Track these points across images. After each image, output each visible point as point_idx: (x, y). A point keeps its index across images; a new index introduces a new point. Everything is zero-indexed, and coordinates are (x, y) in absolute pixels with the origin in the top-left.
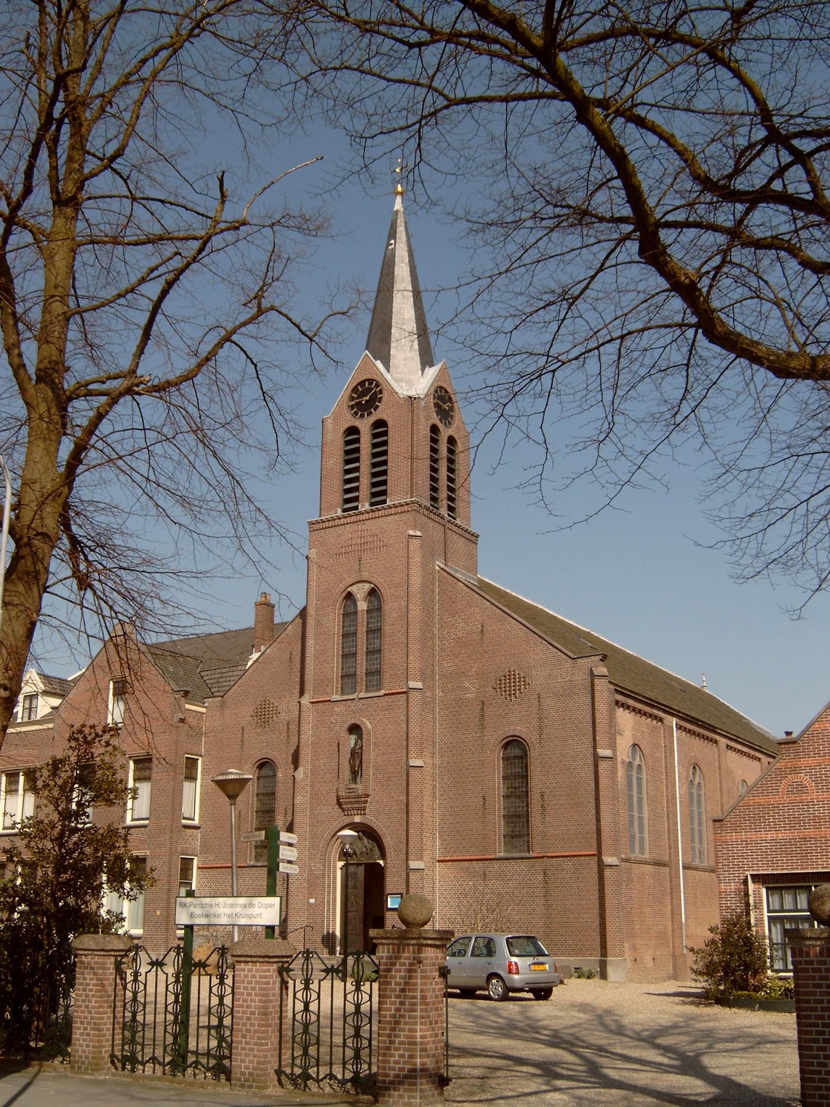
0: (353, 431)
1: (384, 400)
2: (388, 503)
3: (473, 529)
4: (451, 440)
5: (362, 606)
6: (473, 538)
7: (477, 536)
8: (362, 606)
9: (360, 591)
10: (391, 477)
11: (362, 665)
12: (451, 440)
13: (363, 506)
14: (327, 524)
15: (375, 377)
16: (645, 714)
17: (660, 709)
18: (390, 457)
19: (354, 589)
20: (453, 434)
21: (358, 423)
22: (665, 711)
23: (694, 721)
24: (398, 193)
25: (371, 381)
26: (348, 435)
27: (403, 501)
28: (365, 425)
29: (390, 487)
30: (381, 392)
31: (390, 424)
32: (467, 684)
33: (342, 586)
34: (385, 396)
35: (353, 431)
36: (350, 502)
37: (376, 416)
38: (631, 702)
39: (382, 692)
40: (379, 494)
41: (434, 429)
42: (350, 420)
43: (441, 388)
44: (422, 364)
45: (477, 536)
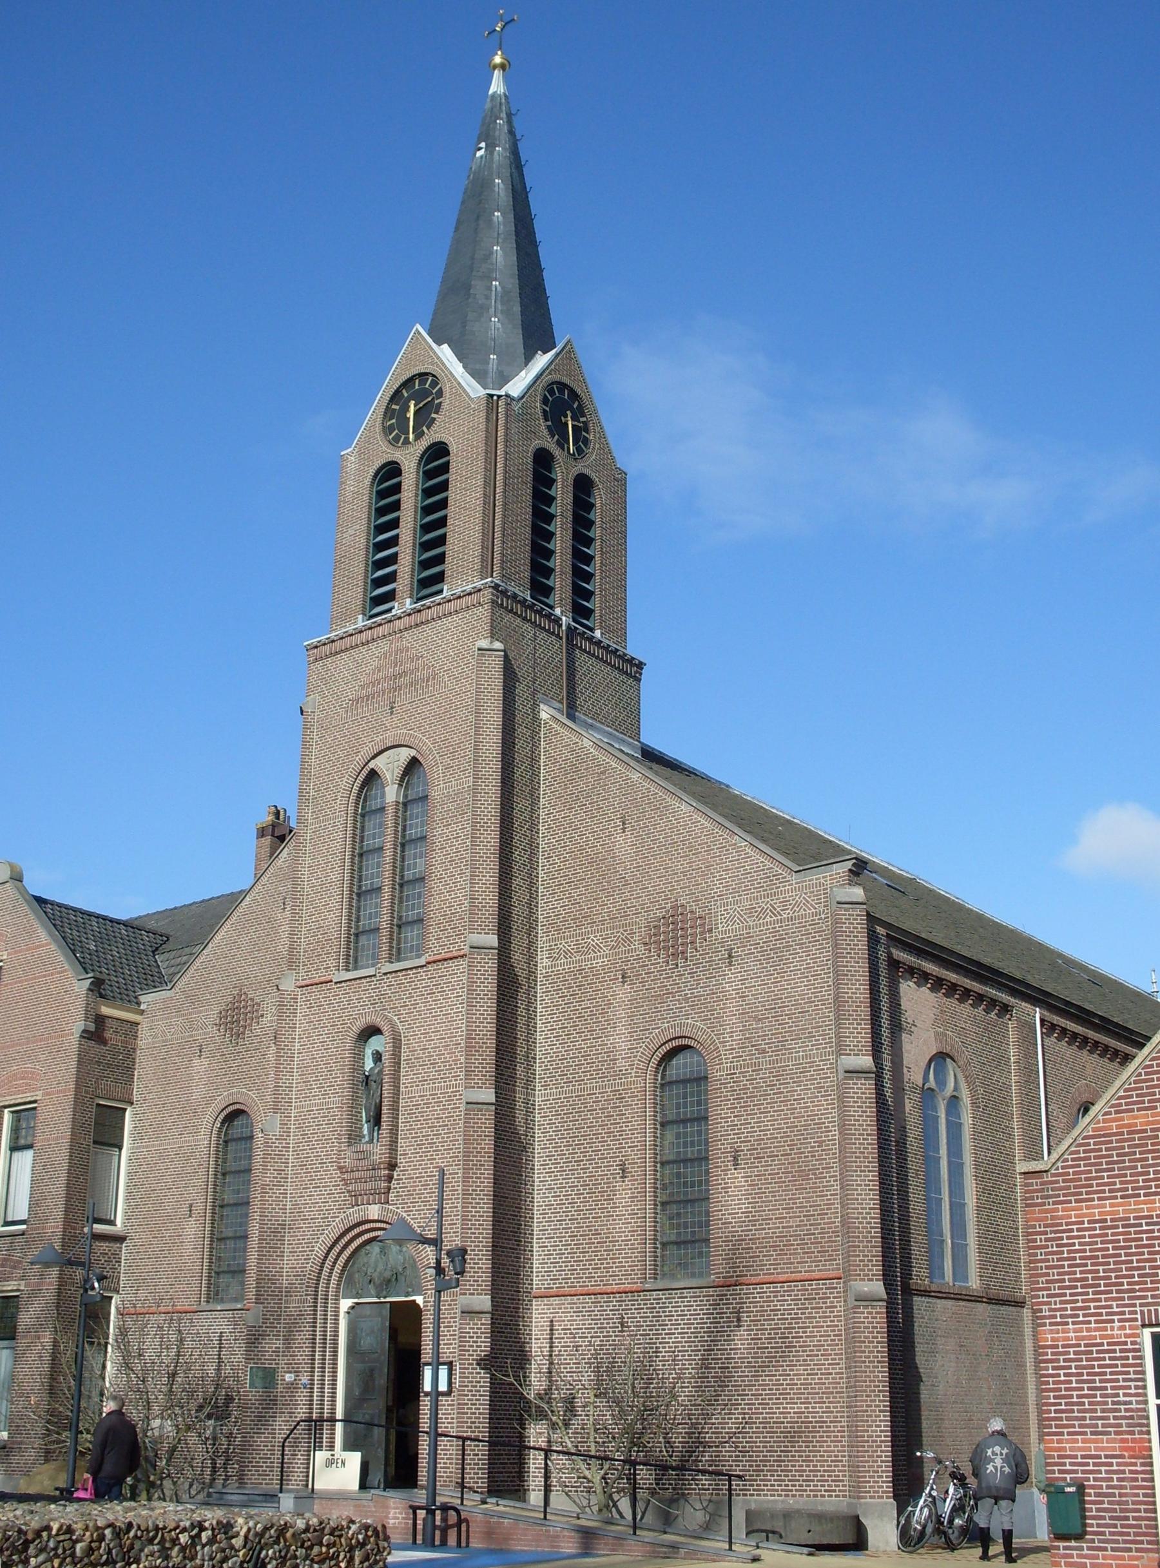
0: (391, 470)
1: (445, 406)
2: (445, 594)
3: (633, 650)
4: (583, 485)
5: (391, 793)
6: (633, 669)
7: (640, 665)
8: (391, 793)
9: (390, 766)
10: (452, 548)
11: (382, 910)
12: (583, 485)
13: (403, 604)
14: (338, 646)
15: (429, 368)
16: (966, 993)
17: (1001, 986)
18: (451, 511)
19: (379, 764)
20: (588, 472)
21: (398, 455)
22: (1014, 992)
23: (1083, 1016)
24: (495, 67)
25: (423, 376)
26: (380, 483)
27: (469, 588)
28: (409, 460)
29: (448, 567)
30: (440, 394)
31: (453, 448)
32: (593, 939)
33: (359, 759)
34: (446, 402)
35: (391, 470)
36: (380, 598)
37: (432, 436)
38: (929, 967)
39: (422, 961)
40: (430, 580)
41: (543, 460)
42: (386, 453)
43: (562, 386)
44: (902, 888)
45: (640, 665)
